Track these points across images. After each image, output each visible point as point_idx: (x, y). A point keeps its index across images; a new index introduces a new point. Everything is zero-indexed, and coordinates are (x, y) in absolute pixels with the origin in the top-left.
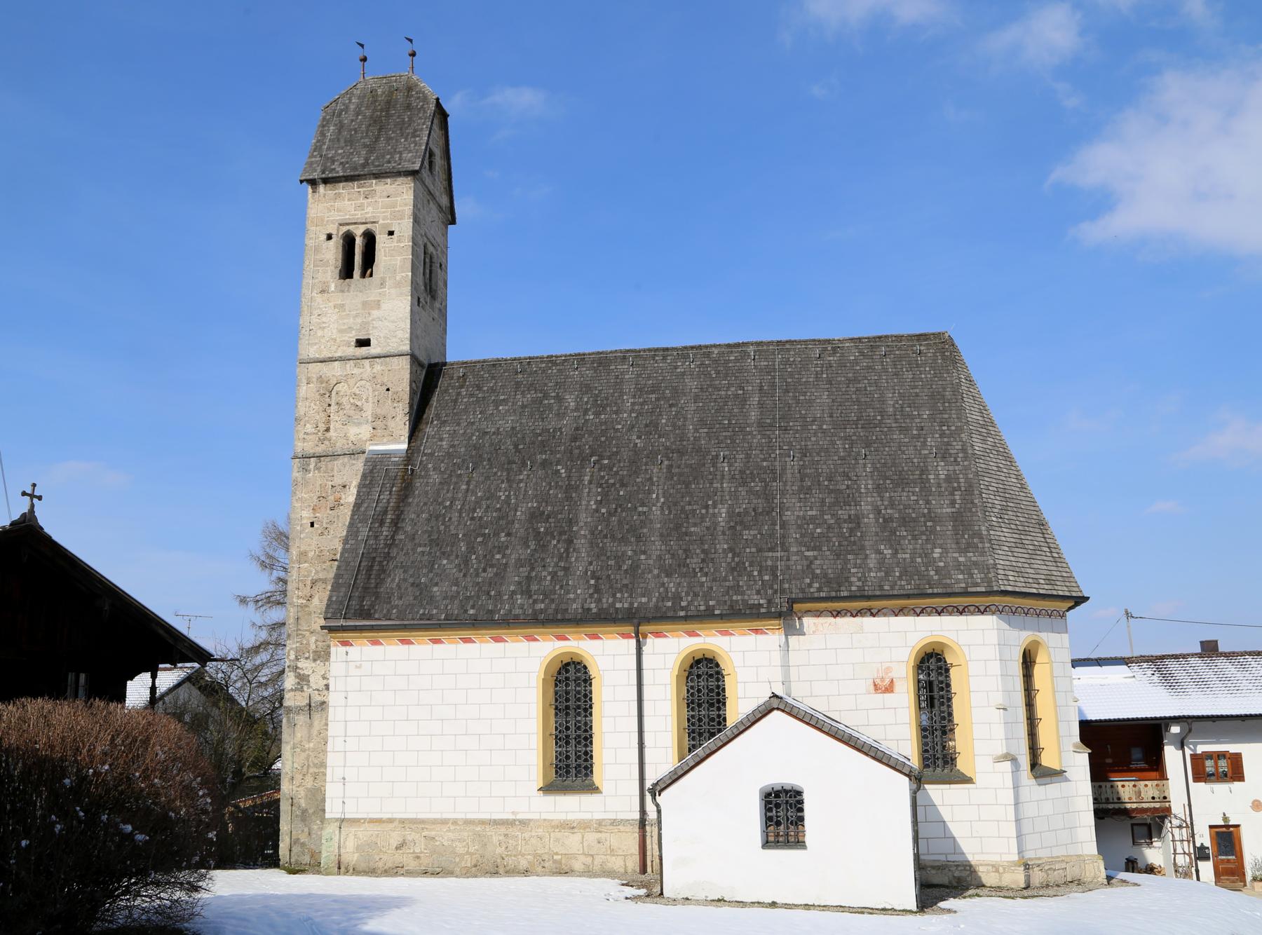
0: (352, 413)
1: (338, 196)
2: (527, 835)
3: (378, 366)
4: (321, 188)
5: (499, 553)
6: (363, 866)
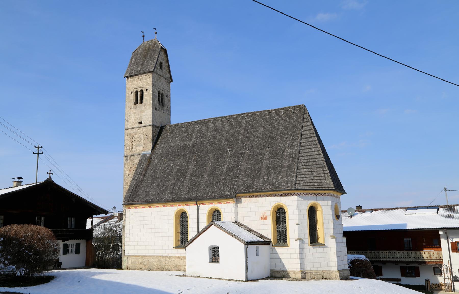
2: (170, 260)
3: (144, 129)
4: (130, 78)
6: (133, 268)
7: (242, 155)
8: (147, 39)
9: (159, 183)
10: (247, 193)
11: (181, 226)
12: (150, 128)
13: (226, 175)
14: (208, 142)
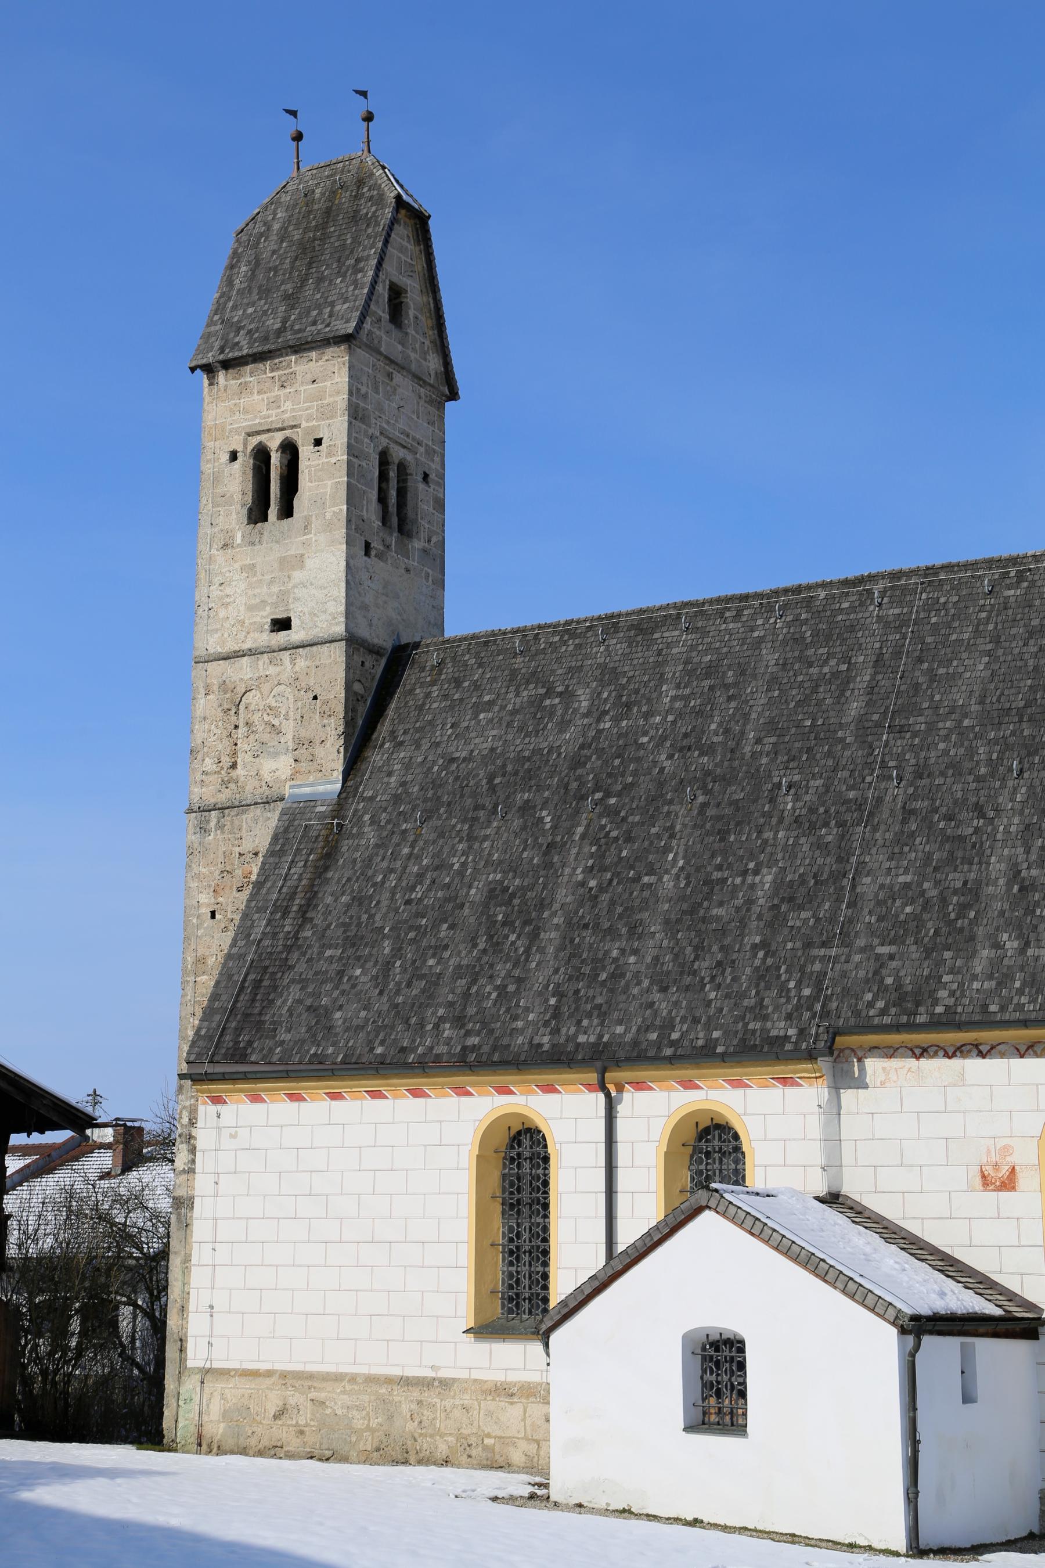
0: (266, 737)
1: (244, 387)
2: (448, 1403)
4: (221, 377)
5: (434, 956)
7: (867, 812)
8: (317, 153)
9: (388, 965)
10: (896, 1028)
11: (512, 1206)
12: (335, 657)
13: (770, 925)
14: (663, 739)
